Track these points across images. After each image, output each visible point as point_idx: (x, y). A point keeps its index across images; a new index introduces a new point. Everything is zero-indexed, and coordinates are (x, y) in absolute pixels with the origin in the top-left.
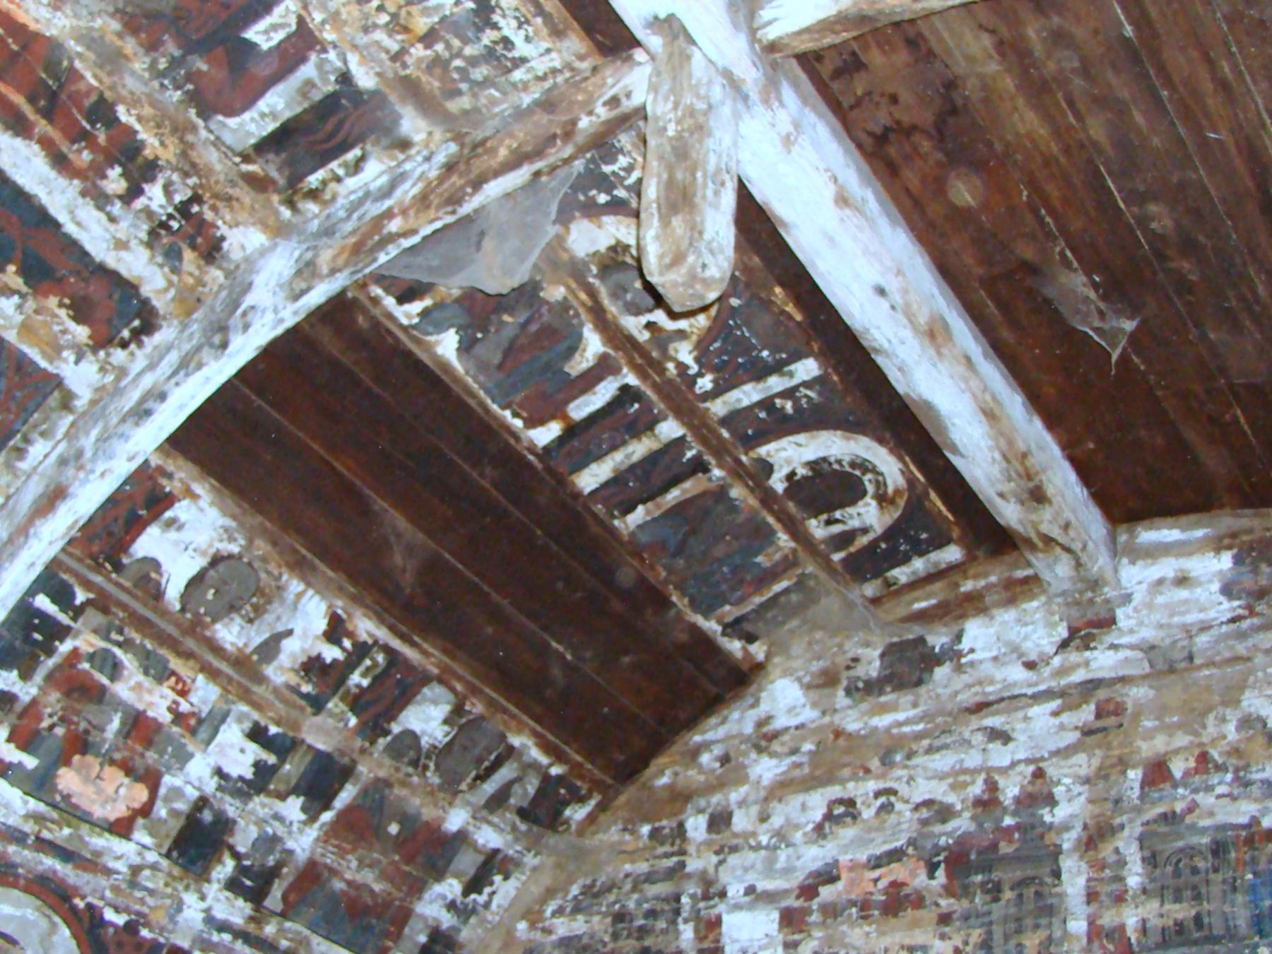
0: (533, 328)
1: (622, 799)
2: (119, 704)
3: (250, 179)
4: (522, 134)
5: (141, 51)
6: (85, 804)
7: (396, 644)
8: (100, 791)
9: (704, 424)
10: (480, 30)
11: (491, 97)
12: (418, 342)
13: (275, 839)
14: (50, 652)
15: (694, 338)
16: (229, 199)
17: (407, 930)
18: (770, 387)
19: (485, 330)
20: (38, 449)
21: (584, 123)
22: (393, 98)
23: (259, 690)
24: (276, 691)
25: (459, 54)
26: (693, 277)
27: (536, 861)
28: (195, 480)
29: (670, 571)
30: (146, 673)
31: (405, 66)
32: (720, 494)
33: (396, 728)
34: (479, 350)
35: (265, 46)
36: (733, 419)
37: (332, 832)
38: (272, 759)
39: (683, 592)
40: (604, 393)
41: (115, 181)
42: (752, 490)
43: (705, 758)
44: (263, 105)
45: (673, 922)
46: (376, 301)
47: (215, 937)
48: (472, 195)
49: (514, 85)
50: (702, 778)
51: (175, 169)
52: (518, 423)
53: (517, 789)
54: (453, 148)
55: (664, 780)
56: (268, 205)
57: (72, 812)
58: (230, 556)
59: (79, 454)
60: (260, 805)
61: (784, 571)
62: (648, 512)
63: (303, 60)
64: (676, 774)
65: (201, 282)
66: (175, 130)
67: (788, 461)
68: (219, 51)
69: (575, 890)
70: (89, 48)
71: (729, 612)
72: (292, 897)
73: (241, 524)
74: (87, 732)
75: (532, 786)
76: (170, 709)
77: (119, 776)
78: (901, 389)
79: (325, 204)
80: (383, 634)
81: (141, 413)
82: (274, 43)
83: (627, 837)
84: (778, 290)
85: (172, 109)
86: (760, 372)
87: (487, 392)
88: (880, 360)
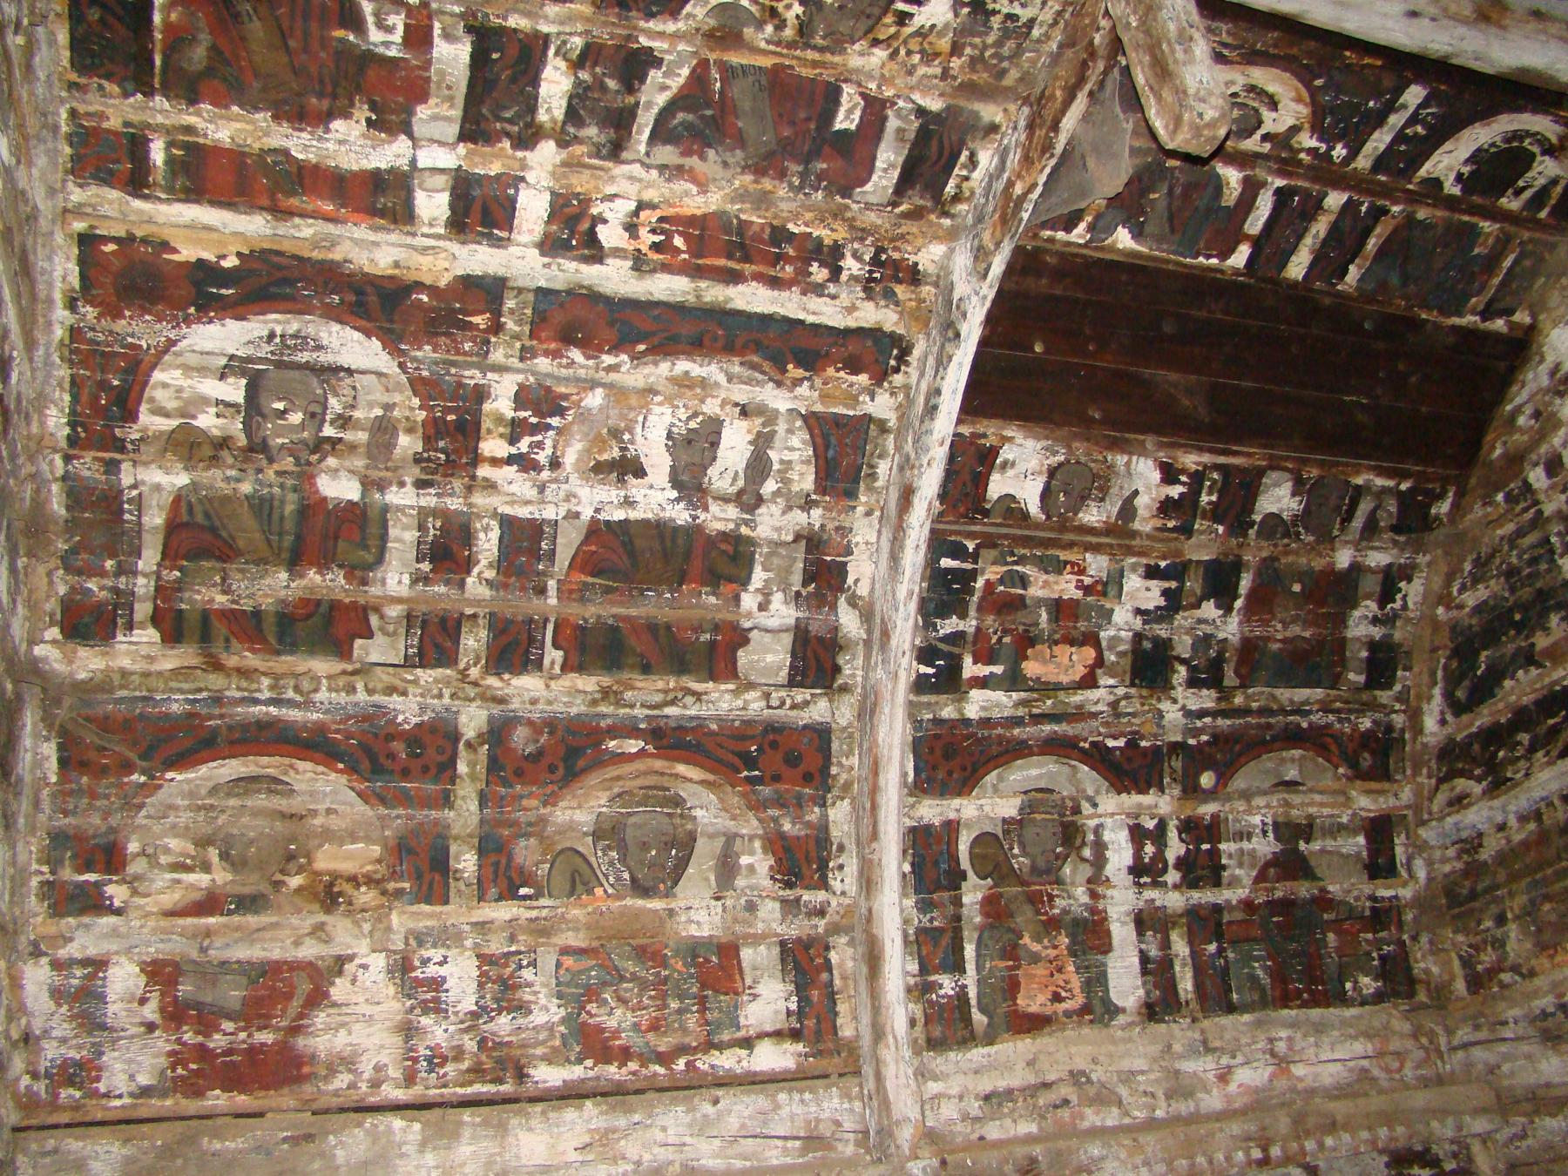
0: (1178, 191)
1: (1473, 481)
2: (1040, 602)
3: (906, 215)
4: (1065, 72)
5: (777, 182)
6: (1053, 679)
7: (1222, 460)
8: (1059, 665)
9: (1362, 181)
10: (986, 23)
11: (1030, 60)
12: (1102, 249)
13: (1207, 638)
14: (971, 592)
15: (1307, 126)
16: (902, 236)
17: (1348, 654)
18: (1394, 125)
19: (1143, 213)
20: (883, 468)
21: (1097, 39)
22: (962, 103)
23: (1136, 542)
24: (1149, 536)
25: (985, 47)
26: (1197, 130)
27: (1428, 557)
28: (1003, 428)
29: (1406, 298)
30: (1047, 572)
31: (955, 78)
32: (1409, 221)
33: (1257, 518)
34: (1148, 229)
35: (853, 127)
36: (1380, 163)
37: (1250, 611)
38: (1173, 585)
39: (1429, 308)
40: (1264, 206)
41: (819, 273)
42: (1434, 206)
43: (1521, 421)
44: (879, 164)
45: (1553, 561)
46: (1051, 240)
47: (1199, 724)
48: (1057, 136)
49: (1038, 41)
50: (1526, 438)
51: (852, 241)
52: (1214, 261)
53: (1380, 513)
54: (1026, 110)
55: (1498, 452)
56: (931, 224)
57: (1048, 688)
58: (1061, 465)
59: (908, 458)
60: (1182, 619)
61: (1505, 248)
62: (1360, 267)
63: (885, 119)
64: (1505, 443)
65: (921, 301)
66: (835, 216)
67: (1450, 169)
68: (827, 149)
69: (1467, 567)
70: (743, 202)
71: (1477, 303)
72: (1243, 671)
73: (1055, 440)
74: (1026, 631)
75: (1392, 506)
76: (1077, 587)
77: (1067, 649)
78: (1489, 70)
79: (968, 200)
80: (1207, 458)
81: (931, 410)
82: (857, 121)
83: (1489, 509)
84: (1348, 54)
85: (823, 206)
86: (1379, 119)
87: (1174, 253)
88: (1455, 61)
